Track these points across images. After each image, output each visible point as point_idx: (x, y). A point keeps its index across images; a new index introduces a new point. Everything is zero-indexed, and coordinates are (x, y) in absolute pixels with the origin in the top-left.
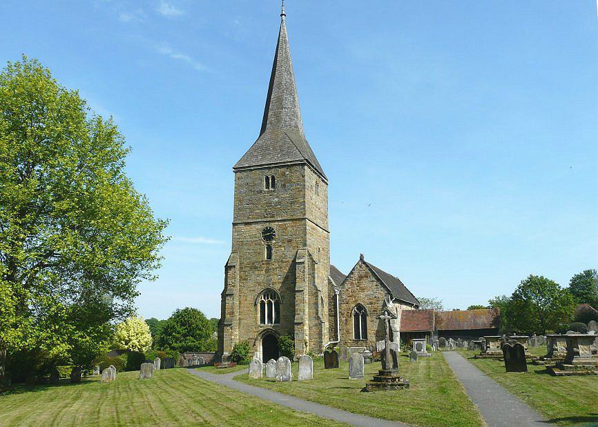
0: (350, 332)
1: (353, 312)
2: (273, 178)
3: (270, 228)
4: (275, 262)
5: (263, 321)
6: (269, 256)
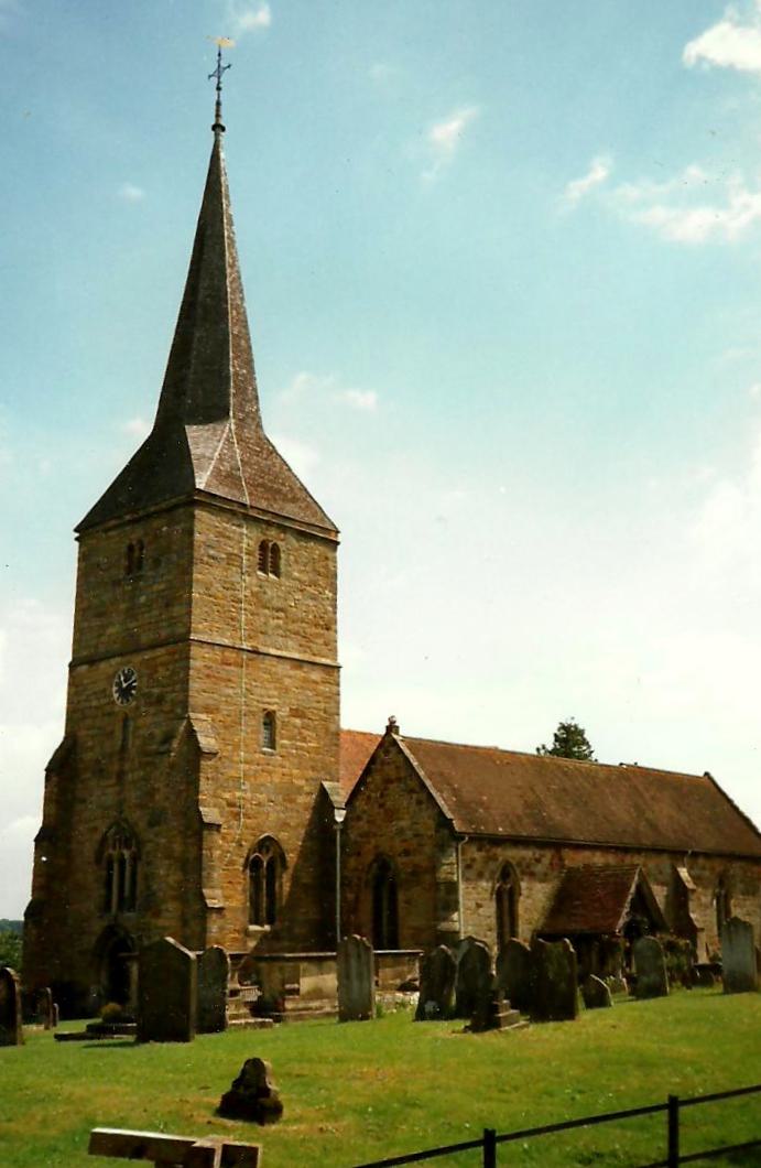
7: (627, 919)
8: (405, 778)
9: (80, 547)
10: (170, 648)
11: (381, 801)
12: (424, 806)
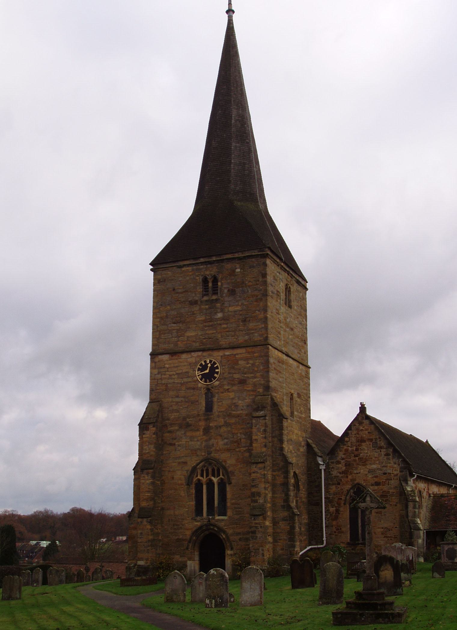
4: (219, 416)
6: (209, 408)
7: (323, 539)
8: (376, 439)
9: (154, 275)
10: (249, 349)
11: (356, 453)
12: (391, 457)
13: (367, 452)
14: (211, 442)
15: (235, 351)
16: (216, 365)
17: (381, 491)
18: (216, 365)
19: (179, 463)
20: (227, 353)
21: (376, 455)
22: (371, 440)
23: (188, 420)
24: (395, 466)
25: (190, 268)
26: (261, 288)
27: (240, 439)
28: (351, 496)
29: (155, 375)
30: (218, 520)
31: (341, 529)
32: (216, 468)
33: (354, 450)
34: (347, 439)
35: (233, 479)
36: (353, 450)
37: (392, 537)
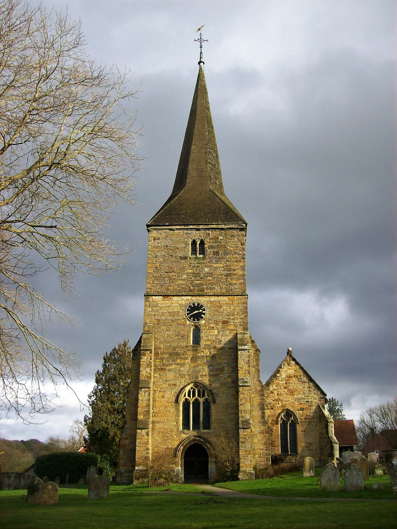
0: (276, 444)
1: (280, 419)
2: (202, 243)
3: (198, 304)
4: (205, 348)
5: (186, 425)
6: (197, 340)
13: (294, 385)
14: (198, 369)
15: (220, 298)
16: (203, 308)
17: (305, 415)
18: (203, 308)
19: (169, 385)
20: (213, 299)
21: (301, 387)
22: (297, 377)
23: (177, 350)
24: (315, 396)
25: (181, 231)
26: (240, 252)
27: (224, 368)
28: (282, 418)
29: (150, 311)
30: (203, 433)
31: (274, 443)
32: (201, 390)
33: (284, 383)
34: (278, 375)
35: (217, 399)
36: (283, 383)
37: (314, 450)
